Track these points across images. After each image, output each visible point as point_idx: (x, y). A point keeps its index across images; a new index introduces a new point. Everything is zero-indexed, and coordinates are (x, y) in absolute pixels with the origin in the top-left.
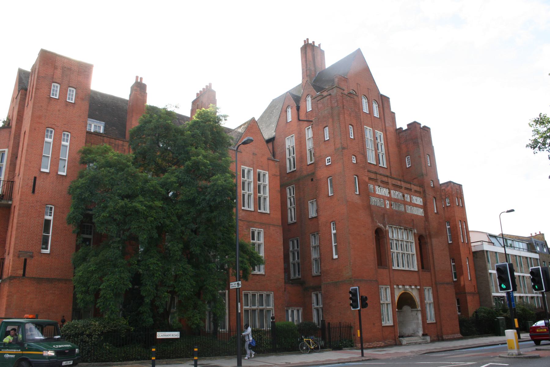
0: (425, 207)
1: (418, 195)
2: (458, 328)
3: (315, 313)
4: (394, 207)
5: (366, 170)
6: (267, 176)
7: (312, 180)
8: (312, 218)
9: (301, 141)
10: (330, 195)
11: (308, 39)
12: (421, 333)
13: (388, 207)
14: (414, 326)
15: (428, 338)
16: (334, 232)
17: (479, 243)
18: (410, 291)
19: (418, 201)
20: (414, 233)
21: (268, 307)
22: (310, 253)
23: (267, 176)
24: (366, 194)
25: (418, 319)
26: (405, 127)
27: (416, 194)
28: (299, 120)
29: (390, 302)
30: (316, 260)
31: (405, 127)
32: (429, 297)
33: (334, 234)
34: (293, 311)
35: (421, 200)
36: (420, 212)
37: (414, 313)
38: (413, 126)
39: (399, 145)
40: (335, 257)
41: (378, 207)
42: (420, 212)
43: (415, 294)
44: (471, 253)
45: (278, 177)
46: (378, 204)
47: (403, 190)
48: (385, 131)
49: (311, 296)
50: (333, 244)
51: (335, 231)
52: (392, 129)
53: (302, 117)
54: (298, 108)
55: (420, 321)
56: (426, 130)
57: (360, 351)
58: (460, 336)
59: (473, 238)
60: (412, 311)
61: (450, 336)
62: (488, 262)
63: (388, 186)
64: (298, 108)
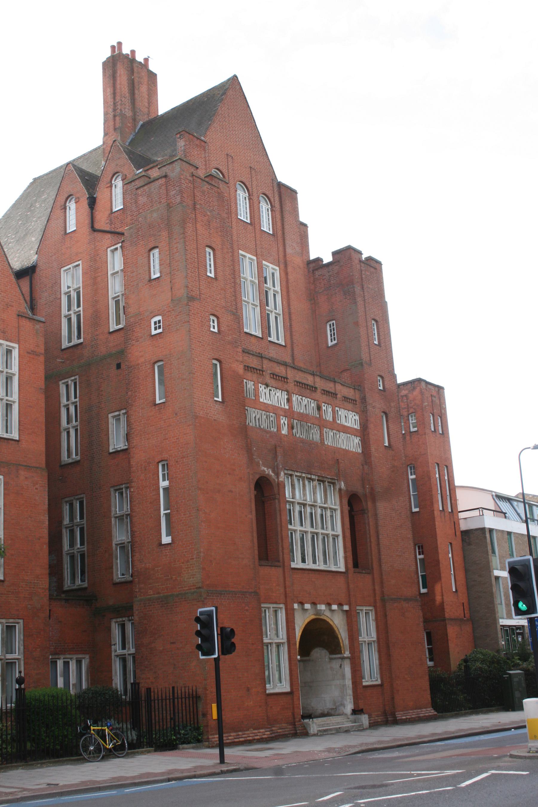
0: (364, 433)
1: (350, 406)
2: (427, 696)
3: (117, 666)
4: (298, 433)
5: (240, 350)
6: (15, 353)
7: (119, 366)
8: (117, 452)
9: (96, 276)
10: (158, 401)
11: (120, 44)
12: (349, 707)
13: (284, 431)
14: (336, 693)
15: (365, 719)
16: (164, 484)
17: (476, 513)
18: (327, 615)
19: (350, 419)
20: (340, 490)
21: (9, 656)
22: (110, 532)
23: (15, 353)
24: (237, 401)
25: (343, 677)
26: (327, 259)
27: (346, 404)
28: (94, 229)
29: (285, 640)
30: (122, 546)
31: (327, 259)
32: (368, 630)
33: (166, 489)
34: (66, 664)
35: (357, 418)
36: (353, 444)
37: (335, 665)
38: (346, 255)
39: (312, 298)
40: (166, 540)
41: (263, 430)
42: (353, 444)
43: (338, 622)
44: (458, 534)
45: (42, 359)
46: (264, 425)
47: (318, 395)
48: (284, 264)
49: (109, 629)
50: (163, 512)
51: (166, 483)
52: (296, 261)
53: (102, 222)
54: (92, 202)
55: (349, 682)
56: (373, 266)
57: (217, 751)
58: (431, 712)
59: (464, 501)
60: (331, 659)
61: (412, 714)
62: (493, 552)
63: (286, 386)
64: (92, 202)
